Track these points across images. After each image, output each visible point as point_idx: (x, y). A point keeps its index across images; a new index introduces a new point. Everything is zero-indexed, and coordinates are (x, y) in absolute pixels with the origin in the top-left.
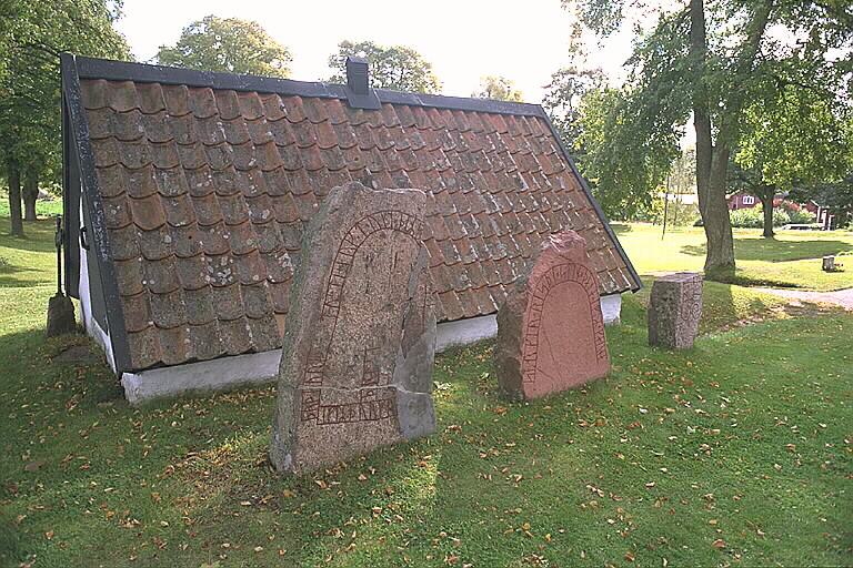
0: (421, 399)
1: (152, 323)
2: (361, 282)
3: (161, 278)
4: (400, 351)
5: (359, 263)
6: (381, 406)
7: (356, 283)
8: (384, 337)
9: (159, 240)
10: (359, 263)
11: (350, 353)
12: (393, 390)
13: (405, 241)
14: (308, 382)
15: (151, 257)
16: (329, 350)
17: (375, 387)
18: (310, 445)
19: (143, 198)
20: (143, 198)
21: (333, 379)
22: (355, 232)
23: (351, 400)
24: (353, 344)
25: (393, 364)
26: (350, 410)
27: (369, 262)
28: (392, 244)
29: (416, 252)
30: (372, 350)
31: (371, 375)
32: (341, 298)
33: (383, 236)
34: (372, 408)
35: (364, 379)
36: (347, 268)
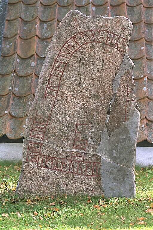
0: (120, 170)
1: (6, 112)
2: (75, 76)
3: (23, 88)
4: (106, 130)
5: (73, 63)
6: (87, 167)
7: (72, 76)
8: (92, 118)
9: (28, 65)
10: (73, 63)
11: (65, 123)
12: (99, 158)
13: (110, 52)
14: (34, 136)
15: (21, 74)
16: (49, 118)
17: (83, 151)
18: (31, 178)
19: (27, 39)
20: (27, 39)
21: (52, 139)
22: (72, 43)
23: (63, 156)
24: (67, 118)
25: (99, 138)
26: (62, 163)
27: (81, 63)
28: (101, 54)
29: (120, 61)
30: (82, 125)
31: (80, 142)
32: (59, 85)
33: (93, 47)
34: (79, 166)
35: (74, 144)
36: (64, 66)
